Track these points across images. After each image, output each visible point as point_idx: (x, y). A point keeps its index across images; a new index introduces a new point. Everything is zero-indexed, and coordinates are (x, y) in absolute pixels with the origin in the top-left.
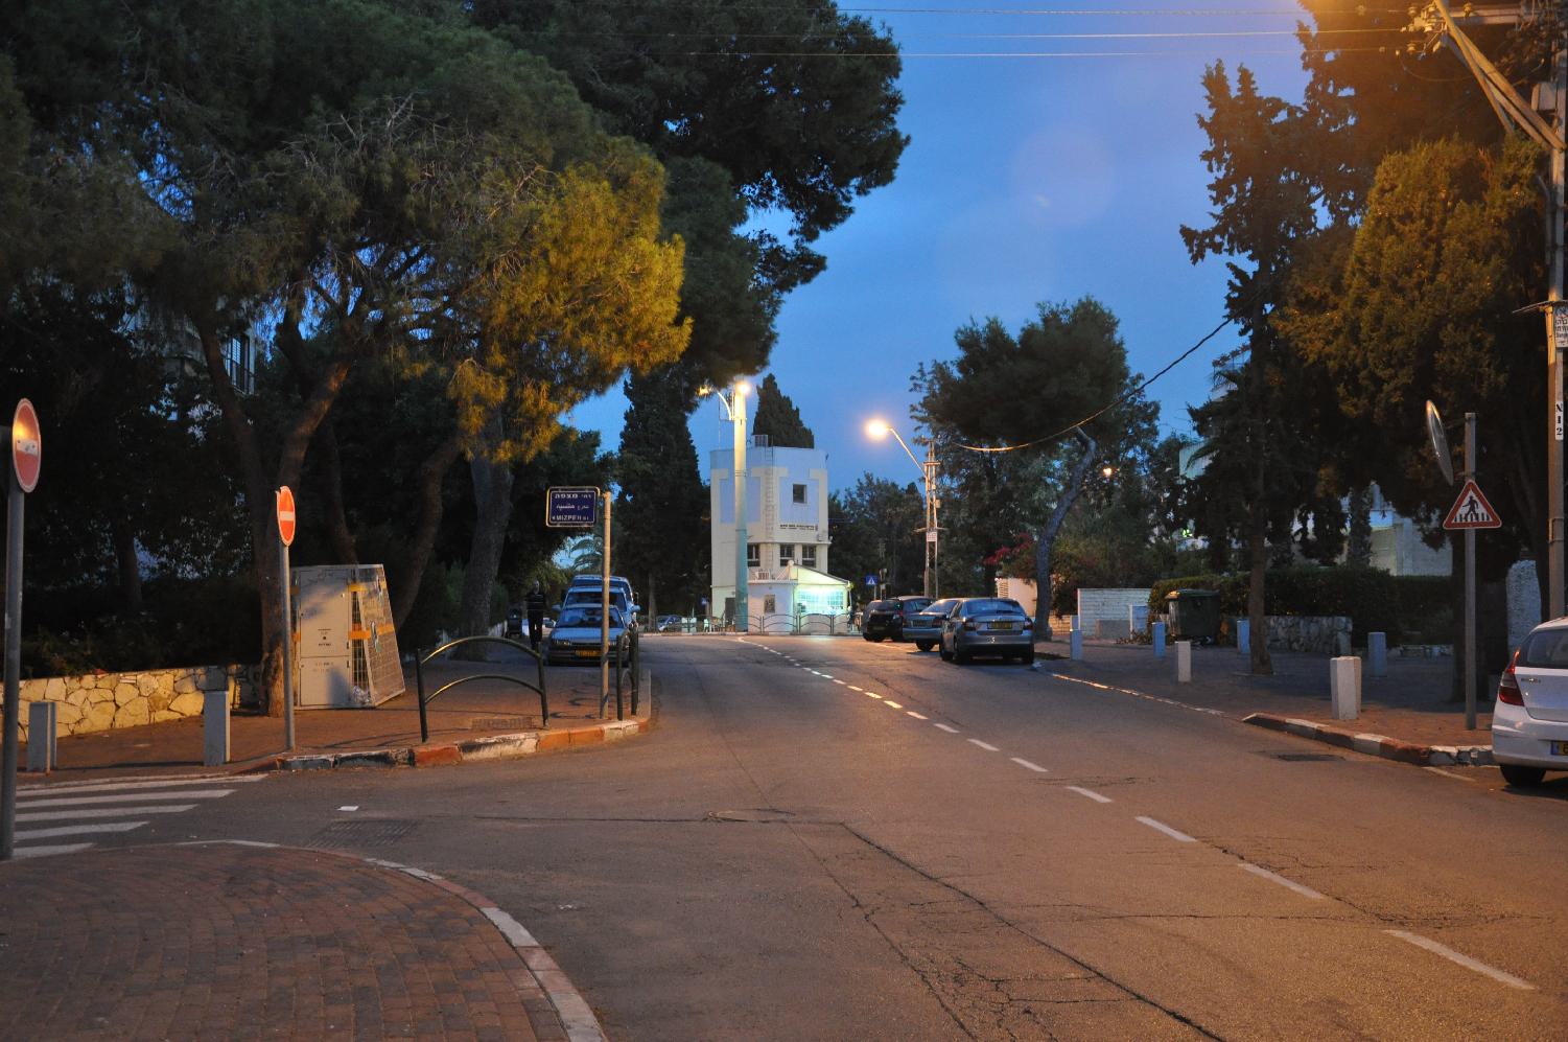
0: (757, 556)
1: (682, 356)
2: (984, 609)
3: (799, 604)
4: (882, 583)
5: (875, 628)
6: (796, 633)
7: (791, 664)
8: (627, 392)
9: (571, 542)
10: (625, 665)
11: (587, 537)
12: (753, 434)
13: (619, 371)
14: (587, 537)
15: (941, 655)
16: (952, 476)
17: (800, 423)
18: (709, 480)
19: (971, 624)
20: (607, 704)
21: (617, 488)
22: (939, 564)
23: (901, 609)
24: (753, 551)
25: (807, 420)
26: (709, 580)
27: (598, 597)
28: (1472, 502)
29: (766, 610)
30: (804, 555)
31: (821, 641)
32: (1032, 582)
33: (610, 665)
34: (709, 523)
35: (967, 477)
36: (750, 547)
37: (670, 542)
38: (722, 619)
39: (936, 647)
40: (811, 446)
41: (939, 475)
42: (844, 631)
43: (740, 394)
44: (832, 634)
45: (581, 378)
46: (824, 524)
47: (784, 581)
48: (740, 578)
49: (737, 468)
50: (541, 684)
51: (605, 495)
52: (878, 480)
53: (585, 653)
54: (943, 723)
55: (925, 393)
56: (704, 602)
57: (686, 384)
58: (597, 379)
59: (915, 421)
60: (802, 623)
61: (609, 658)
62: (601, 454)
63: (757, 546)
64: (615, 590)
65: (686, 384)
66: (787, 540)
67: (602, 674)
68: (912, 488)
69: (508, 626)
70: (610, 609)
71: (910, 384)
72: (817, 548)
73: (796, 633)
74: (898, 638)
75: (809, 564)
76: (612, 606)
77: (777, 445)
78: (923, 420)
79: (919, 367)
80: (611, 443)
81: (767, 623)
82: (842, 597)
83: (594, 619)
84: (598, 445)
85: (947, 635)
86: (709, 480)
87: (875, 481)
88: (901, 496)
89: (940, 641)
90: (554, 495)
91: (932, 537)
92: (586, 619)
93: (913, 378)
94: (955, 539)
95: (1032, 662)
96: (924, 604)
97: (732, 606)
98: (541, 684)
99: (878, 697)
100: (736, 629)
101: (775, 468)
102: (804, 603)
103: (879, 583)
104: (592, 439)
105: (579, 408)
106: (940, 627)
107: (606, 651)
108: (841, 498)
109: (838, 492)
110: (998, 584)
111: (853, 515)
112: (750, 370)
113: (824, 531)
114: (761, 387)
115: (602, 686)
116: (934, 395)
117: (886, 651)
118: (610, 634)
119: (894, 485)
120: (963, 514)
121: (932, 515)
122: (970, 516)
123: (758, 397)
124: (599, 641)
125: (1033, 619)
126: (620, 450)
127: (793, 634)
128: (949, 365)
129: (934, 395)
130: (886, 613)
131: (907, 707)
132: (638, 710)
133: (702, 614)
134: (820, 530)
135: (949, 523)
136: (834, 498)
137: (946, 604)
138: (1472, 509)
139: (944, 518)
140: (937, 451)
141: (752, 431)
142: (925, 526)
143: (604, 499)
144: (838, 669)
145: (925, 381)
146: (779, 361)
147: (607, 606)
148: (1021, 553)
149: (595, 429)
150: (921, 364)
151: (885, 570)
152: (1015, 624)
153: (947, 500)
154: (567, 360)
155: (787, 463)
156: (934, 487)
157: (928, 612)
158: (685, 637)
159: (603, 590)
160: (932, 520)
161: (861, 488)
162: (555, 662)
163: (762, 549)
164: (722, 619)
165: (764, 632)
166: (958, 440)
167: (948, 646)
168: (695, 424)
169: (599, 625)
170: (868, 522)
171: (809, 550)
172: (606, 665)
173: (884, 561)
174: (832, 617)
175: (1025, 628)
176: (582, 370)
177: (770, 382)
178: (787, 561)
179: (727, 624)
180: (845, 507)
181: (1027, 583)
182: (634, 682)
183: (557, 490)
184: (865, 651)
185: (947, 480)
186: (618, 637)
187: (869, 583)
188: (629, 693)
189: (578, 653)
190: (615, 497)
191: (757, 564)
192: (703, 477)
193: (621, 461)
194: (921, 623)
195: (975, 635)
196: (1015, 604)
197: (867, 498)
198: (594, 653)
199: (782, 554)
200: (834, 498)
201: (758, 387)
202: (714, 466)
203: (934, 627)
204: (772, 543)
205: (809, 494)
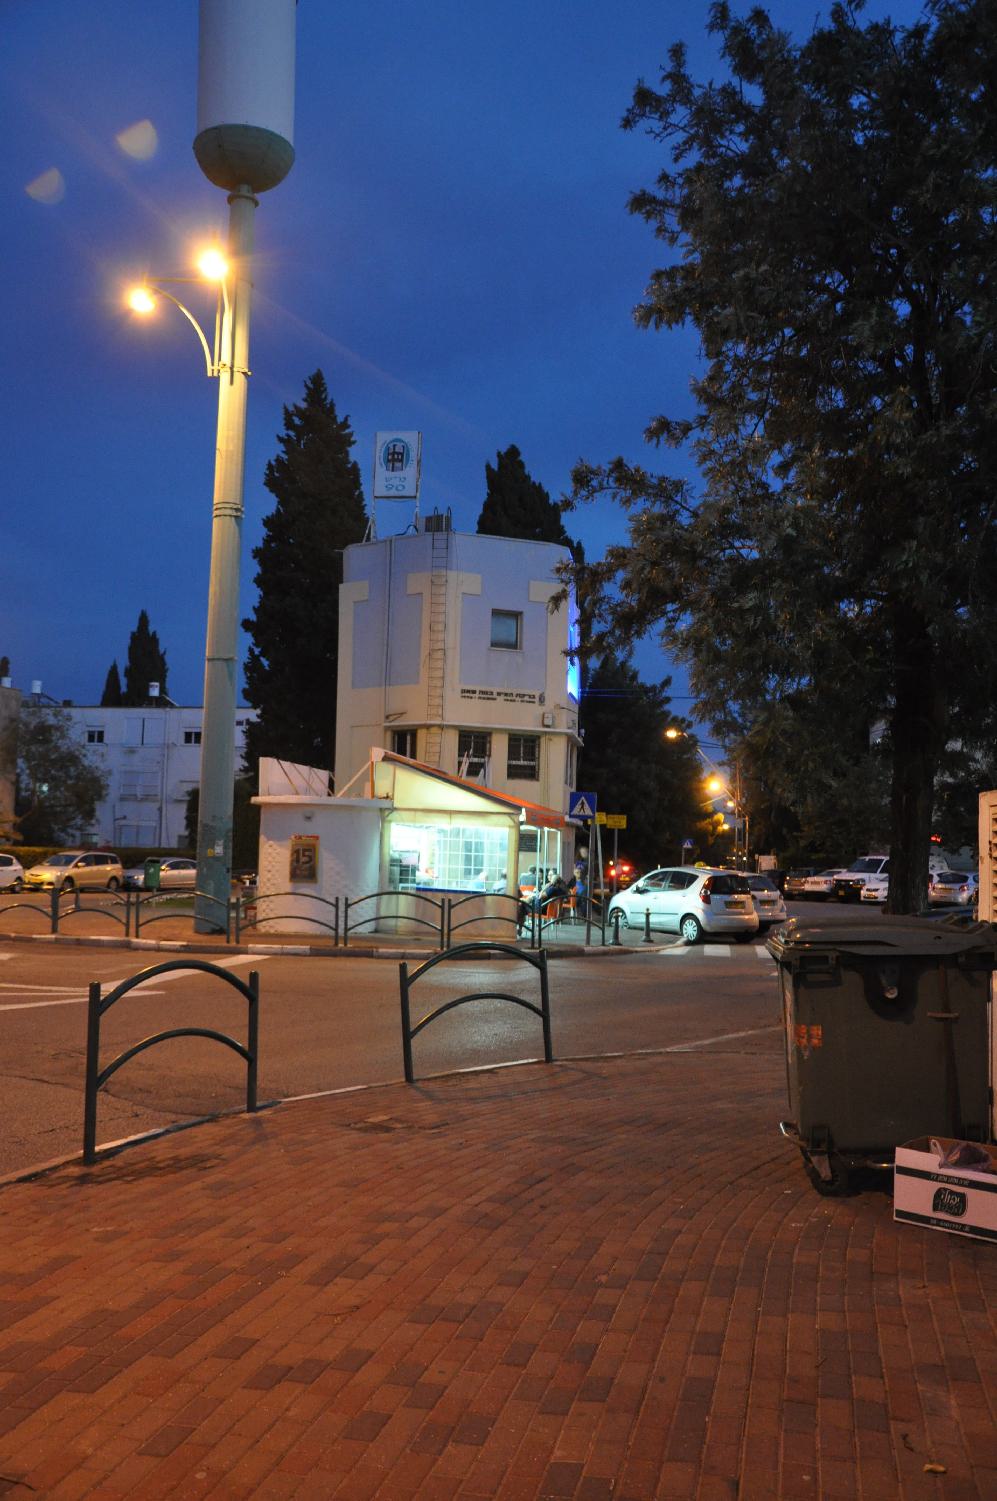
28: (583, 803)
29: (295, 876)
30: (513, 754)
49: (217, 498)
53: (409, 741)
63: (413, 732)
72: (543, 740)
101: (452, 575)
114: (495, 466)
138: (582, 807)
163: (421, 735)
171: (525, 751)
204: (441, 727)
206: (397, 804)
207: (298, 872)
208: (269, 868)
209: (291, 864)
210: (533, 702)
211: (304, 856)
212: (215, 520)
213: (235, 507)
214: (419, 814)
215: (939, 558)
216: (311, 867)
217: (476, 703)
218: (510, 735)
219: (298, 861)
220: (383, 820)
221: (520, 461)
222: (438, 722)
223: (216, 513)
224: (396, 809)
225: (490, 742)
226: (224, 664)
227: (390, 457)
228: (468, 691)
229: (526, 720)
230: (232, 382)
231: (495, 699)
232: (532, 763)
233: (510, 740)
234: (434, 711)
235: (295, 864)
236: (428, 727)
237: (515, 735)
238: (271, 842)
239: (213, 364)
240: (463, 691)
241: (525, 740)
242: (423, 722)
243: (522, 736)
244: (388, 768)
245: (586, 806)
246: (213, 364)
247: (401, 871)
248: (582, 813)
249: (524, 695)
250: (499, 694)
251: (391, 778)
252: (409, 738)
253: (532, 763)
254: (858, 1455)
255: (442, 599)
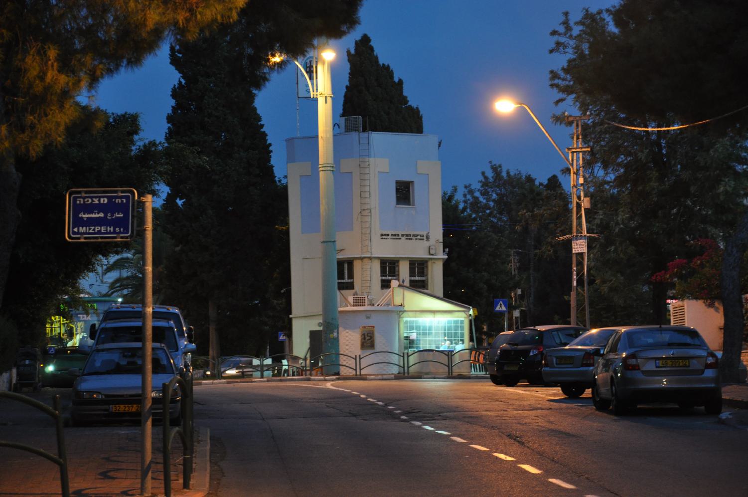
0: (351, 276)
1: (243, 12)
2: (650, 341)
3: (407, 338)
4: (515, 308)
5: (506, 368)
6: (403, 375)
7: (396, 417)
8: (174, 61)
9: (106, 261)
10: (175, 422)
11: (125, 255)
12: (343, 115)
13: (157, 34)
14: (125, 255)
15: (596, 404)
16: (605, 166)
17: (404, 100)
18: (286, 177)
19: (633, 362)
20: (150, 474)
21: (164, 190)
22: (591, 282)
23: (541, 341)
24: (344, 272)
25: (413, 96)
26: (288, 308)
27: (138, 333)
28: (501, 304)
30: (412, 273)
31: (436, 387)
32: (716, 304)
33: (154, 424)
34: (287, 233)
35: (627, 166)
36: (340, 263)
37: (234, 258)
38: (305, 359)
39: (588, 393)
40: (419, 130)
41: (588, 164)
42: (464, 371)
43: (324, 63)
44: (450, 376)
45: (105, 43)
46: (437, 232)
47: (385, 308)
48: (328, 305)
49: (321, 160)
50: (61, 454)
51: (144, 199)
52: (508, 173)
53: (122, 408)
54: (556, 478)
55: (570, 55)
56: (282, 338)
57: (250, 51)
58: (131, 47)
59: (555, 90)
60: (411, 363)
61: (154, 415)
62: (141, 144)
64: (162, 324)
65: (250, 51)
66: (388, 254)
67: (143, 435)
68: (554, 183)
69: (18, 374)
70: (153, 349)
71: (551, 42)
72: (430, 264)
73: (403, 375)
74: (537, 381)
75: (419, 285)
76: (158, 345)
77: (375, 129)
78: (567, 90)
79: (563, 18)
80: (154, 130)
81: (364, 363)
82: (462, 328)
83: (134, 363)
84: (137, 133)
85: (601, 376)
86: (286, 177)
87: (504, 174)
88: (539, 194)
89: (593, 384)
90: (75, 199)
91: (580, 247)
92: (123, 362)
93: (554, 33)
94: (613, 248)
95: (719, 412)
96: (571, 335)
97: (321, 343)
98: (61, 454)
99: (509, 459)
100: (325, 372)
101: (372, 160)
102: (413, 336)
103: (511, 308)
104: (128, 124)
105: (106, 84)
106: (593, 365)
107: (149, 404)
108: (459, 197)
109: (455, 189)
110: (671, 307)
111: (475, 219)
112: (333, 32)
113: (437, 241)
114: (353, 51)
115: (142, 451)
116: (582, 56)
117: (521, 398)
118: (152, 385)
119: (530, 180)
120: (622, 215)
121: (579, 218)
122: (631, 218)
123: (348, 66)
124: (140, 392)
125: (719, 354)
126: (167, 139)
127: (398, 377)
128: (605, 16)
129: (582, 56)
130: (520, 347)
131: (548, 473)
132: (192, 482)
133: (279, 351)
134: (432, 241)
135: (604, 228)
136: (450, 198)
137: (599, 334)
138: (501, 306)
139: (597, 221)
140: (586, 133)
141: (341, 111)
142: (571, 233)
143: (144, 203)
144: (455, 422)
145: (571, 36)
146: (370, 19)
147: (149, 345)
148: (702, 265)
149: (131, 111)
150: (566, 14)
151: (519, 292)
152: (695, 361)
153: (599, 197)
154: (86, 18)
155: (387, 154)
156: (581, 181)
157: (576, 346)
158: (236, 381)
159: (144, 323)
160: (579, 224)
161: (485, 183)
162: (81, 421)
163: (357, 266)
164: (305, 359)
165: (362, 374)
166: (615, 118)
167: (604, 390)
168: (264, 101)
169: (139, 370)
170: (496, 229)
172: (149, 423)
173: (517, 278)
174: (449, 354)
175: (708, 366)
176: (109, 32)
177: (365, 41)
178: (389, 281)
179: (312, 365)
180: (464, 209)
181: (711, 305)
182: (187, 445)
183: (79, 192)
184: (493, 398)
185: (599, 172)
186: (164, 385)
187: (498, 308)
188: (180, 460)
189: (113, 408)
190: (159, 202)
191: (350, 286)
192: (278, 173)
193: (167, 152)
194: (568, 359)
195: (639, 375)
196: (694, 334)
197: (494, 196)
198: (134, 408)
199: (383, 273)
200: (450, 198)
201: (348, 52)
202: (291, 158)
203: (583, 365)
204: (370, 258)
205: (417, 193)
206: (406, 308)
207: (365, 344)
208: (347, 343)
209: (361, 341)
210: (423, 239)
211: (368, 336)
212: (321, 173)
213: (332, 165)
214: (418, 313)
215: (665, 226)
216: (372, 341)
217: (389, 242)
218: (410, 261)
219: (365, 339)
220: (400, 317)
221: (371, 45)
222: (369, 255)
223: (321, 169)
224: (405, 311)
225: (398, 266)
226: (332, 243)
227: (308, 70)
228: (385, 235)
229: (419, 251)
230: (326, 102)
231: (400, 239)
232: (423, 278)
233: (410, 264)
234: (365, 249)
235: (363, 340)
236: (362, 259)
237: (383, 260)
238: (347, 331)
239: (313, 92)
240: (382, 235)
241: (389, 263)
242: (359, 256)
243: (417, 261)
244: (400, 290)
245: (503, 306)
246: (313, 92)
247: (410, 342)
248: (501, 309)
249: (417, 235)
250: (403, 235)
251: (402, 296)
252: (346, 266)
253: (423, 278)
254: (656, 129)
255: (367, 177)
